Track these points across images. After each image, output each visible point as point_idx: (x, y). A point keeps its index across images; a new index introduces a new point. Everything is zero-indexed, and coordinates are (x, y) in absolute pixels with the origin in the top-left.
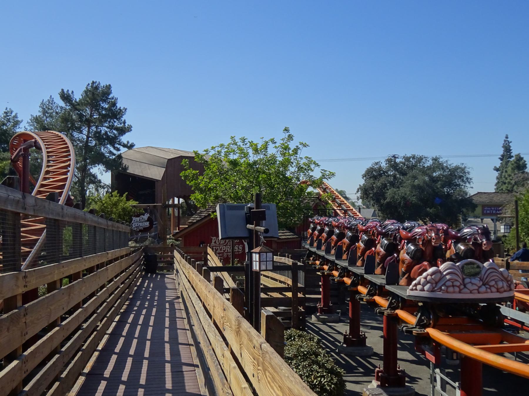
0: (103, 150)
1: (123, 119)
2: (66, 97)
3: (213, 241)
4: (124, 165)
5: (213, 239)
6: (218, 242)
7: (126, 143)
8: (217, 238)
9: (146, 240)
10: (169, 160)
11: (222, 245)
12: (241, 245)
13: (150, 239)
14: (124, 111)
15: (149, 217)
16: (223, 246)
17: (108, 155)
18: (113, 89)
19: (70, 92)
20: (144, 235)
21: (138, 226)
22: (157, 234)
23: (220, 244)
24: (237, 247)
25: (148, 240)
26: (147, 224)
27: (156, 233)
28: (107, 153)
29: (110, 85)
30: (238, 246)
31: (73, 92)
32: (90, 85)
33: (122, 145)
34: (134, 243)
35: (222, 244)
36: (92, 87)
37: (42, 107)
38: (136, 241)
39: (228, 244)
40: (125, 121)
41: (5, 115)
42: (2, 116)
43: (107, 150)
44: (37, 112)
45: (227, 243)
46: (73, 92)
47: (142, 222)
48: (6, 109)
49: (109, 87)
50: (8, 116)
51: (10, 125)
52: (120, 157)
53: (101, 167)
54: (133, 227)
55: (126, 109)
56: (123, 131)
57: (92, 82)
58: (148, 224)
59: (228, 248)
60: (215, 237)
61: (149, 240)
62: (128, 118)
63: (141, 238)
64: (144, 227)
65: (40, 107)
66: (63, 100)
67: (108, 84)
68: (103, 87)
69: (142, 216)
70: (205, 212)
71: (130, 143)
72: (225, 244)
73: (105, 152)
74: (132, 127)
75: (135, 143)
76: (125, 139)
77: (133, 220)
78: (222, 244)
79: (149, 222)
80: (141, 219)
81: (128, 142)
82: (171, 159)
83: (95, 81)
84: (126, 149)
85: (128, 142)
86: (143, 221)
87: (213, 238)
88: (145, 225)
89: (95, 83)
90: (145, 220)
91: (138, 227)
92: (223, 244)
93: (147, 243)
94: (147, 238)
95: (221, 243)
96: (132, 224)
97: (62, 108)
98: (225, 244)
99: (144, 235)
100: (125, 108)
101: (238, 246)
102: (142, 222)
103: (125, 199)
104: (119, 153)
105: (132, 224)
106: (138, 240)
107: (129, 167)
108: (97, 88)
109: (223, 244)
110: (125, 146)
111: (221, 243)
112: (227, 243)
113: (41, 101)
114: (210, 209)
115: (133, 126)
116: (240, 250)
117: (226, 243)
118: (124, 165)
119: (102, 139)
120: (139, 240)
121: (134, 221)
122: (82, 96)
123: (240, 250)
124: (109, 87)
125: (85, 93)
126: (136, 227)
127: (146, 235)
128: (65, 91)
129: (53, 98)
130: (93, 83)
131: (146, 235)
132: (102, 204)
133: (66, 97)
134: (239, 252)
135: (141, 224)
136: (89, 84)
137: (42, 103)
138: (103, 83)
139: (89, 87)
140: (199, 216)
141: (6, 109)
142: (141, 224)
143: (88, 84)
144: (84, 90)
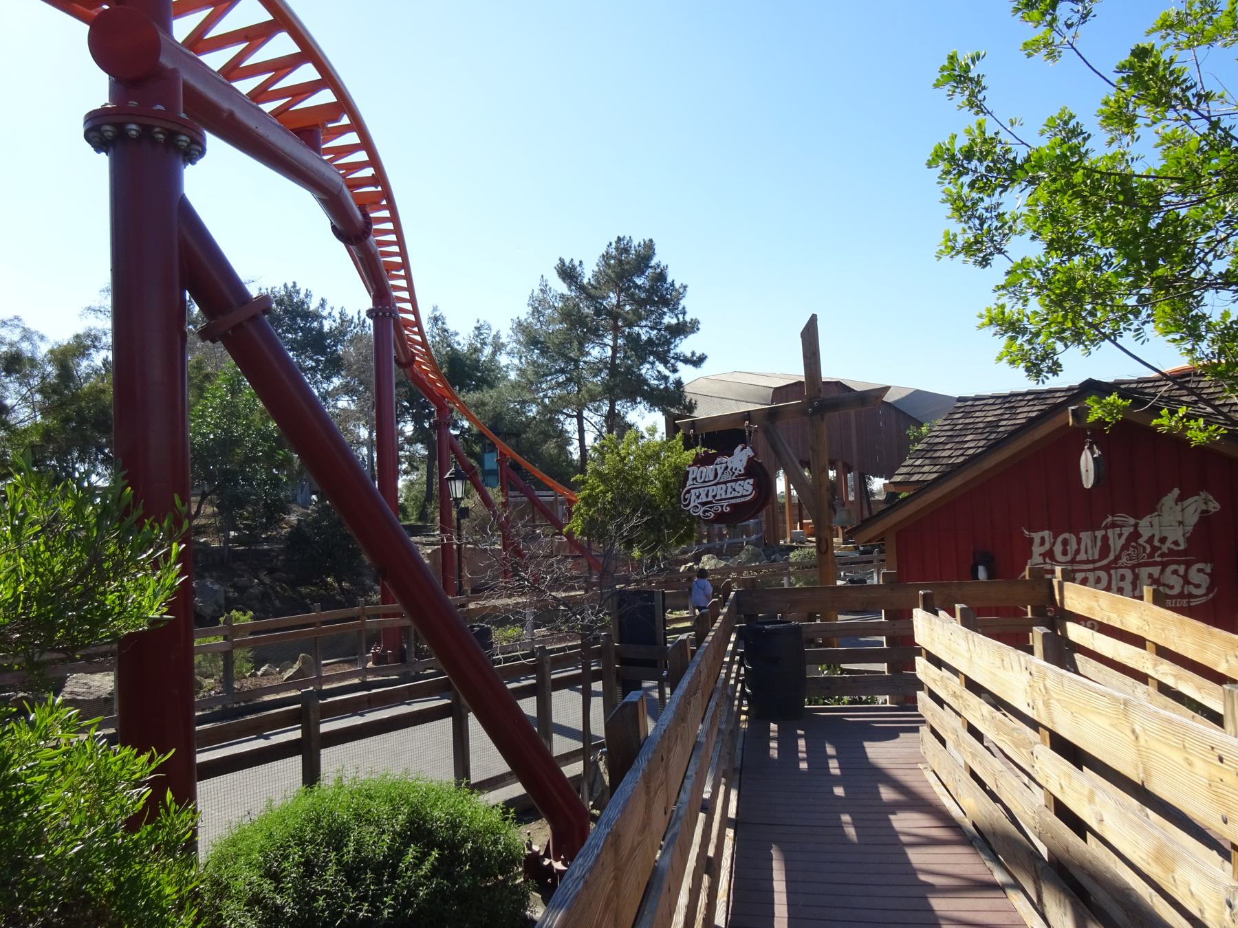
0: (645, 369)
1: (680, 307)
2: (568, 273)
3: (1037, 550)
4: (687, 400)
5: (1037, 540)
6: (1065, 553)
7: (689, 355)
8: (1055, 538)
9: (740, 551)
10: (776, 389)
11: (1091, 566)
12: (1200, 566)
13: (750, 547)
14: (681, 290)
15: (750, 460)
16: (1094, 570)
17: (656, 382)
18: (658, 249)
19: (576, 263)
20: (736, 540)
21: (710, 499)
22: (761, 537)
23: (1073, 561)
24: (1175, 572)
25: (744, 551)
26: (746, 488)
27: (760, 535)
28: (655, 379)
29: (651, 241)
30: (1182, 569)
31: (581, 262)
32: (614, 245)
33: (681, 361)
34: (714, 558)
35: (1087, 562)
36: (617, 249)
37: (532, 305)
38: (719, 554)
39: (1124, 559)
40: (684, 308)
41: (477, 333)
42: (472, 335)
43: (650, 371)
44: (523, 312)
45: (1118, 558)
46: (581, 262)
47: (725, 483)
48: (478, 321)
49: (649, 246)
50: (482, 334)
51: (488, 350)
52: (679, 383)
53: (642, 407)
54: (692, 504)
55: (685, 287)
56: (682, 329)
57: (616, 239)
58: (750, 488)
59: (1123, 578)
60: (1046, 533)
61: (748, 550)
62: (692, 306)
63: (729, 546)
64: (733, 501)
65: (528, 305)
66: (564, 279)
67: (647, 240)
68: (639, 246)
69: (724, 459)
70: (948, 446)
71: (698, 355)
72: (1105, 562)
73: (649, 377)
74: (699, 323)
75: (706, 354)
76: (685, 346)
77: (691, 476)
78: (1087, 562)
79: (751, 481)
80: (720, 472)
81: (693, 354)
82: (779, 388)
83: (621, 236)
84: (690, 367)
85: (693, 354)
86: (727, 477)
87: (1037, 537)
88: (736, 494)
89: (623, 240)
90: (737, 473)
91: (711, 502)
92: (1094, 562)
93: (744, 556)
94: (742, 547)
95: (1079, 558)
96: (688, 492)
97: (562, 296)
98: (1105, 562)
99: (736, 540)
100: (684, 284)
101: (1182, 569)
102: (725, 483)
103: (680, 443)
104: (677, 375)
105: (688, 492)
106: (724, 551)
107: (698, 403)
108: (626, 250)
109: (1094, 562)
110: (686, 361)
111: (1079, 558)
112: (1118, 558)
113: (530, 294)
114: (966, 435)
115: (700, 321)
116: (1198, 586)
117: (1112, 557)
118: (687, 400)
119: (642, 350)
120: (727, 551)
121: (695, 479)
122: (598, 265)
123: (1198, 586)
124: (649, 246)
125: (604, 260)
126: (703, 504)
127: (740, 540)
128: (567, 262)
129: (546, 281)
130: (619, 239)
131: (740, 540)
132: (619, 458)
133: (568, 273)
134: (1191, 596)
135: (720, 491)
136: (611, 244)
137: (532, 297)
138: (637, 240)
139: (613, 251)
140: (927, 462)
141: (478, 321)
142: (720, 491)
143: (608, 243)
144: (601, 254)
